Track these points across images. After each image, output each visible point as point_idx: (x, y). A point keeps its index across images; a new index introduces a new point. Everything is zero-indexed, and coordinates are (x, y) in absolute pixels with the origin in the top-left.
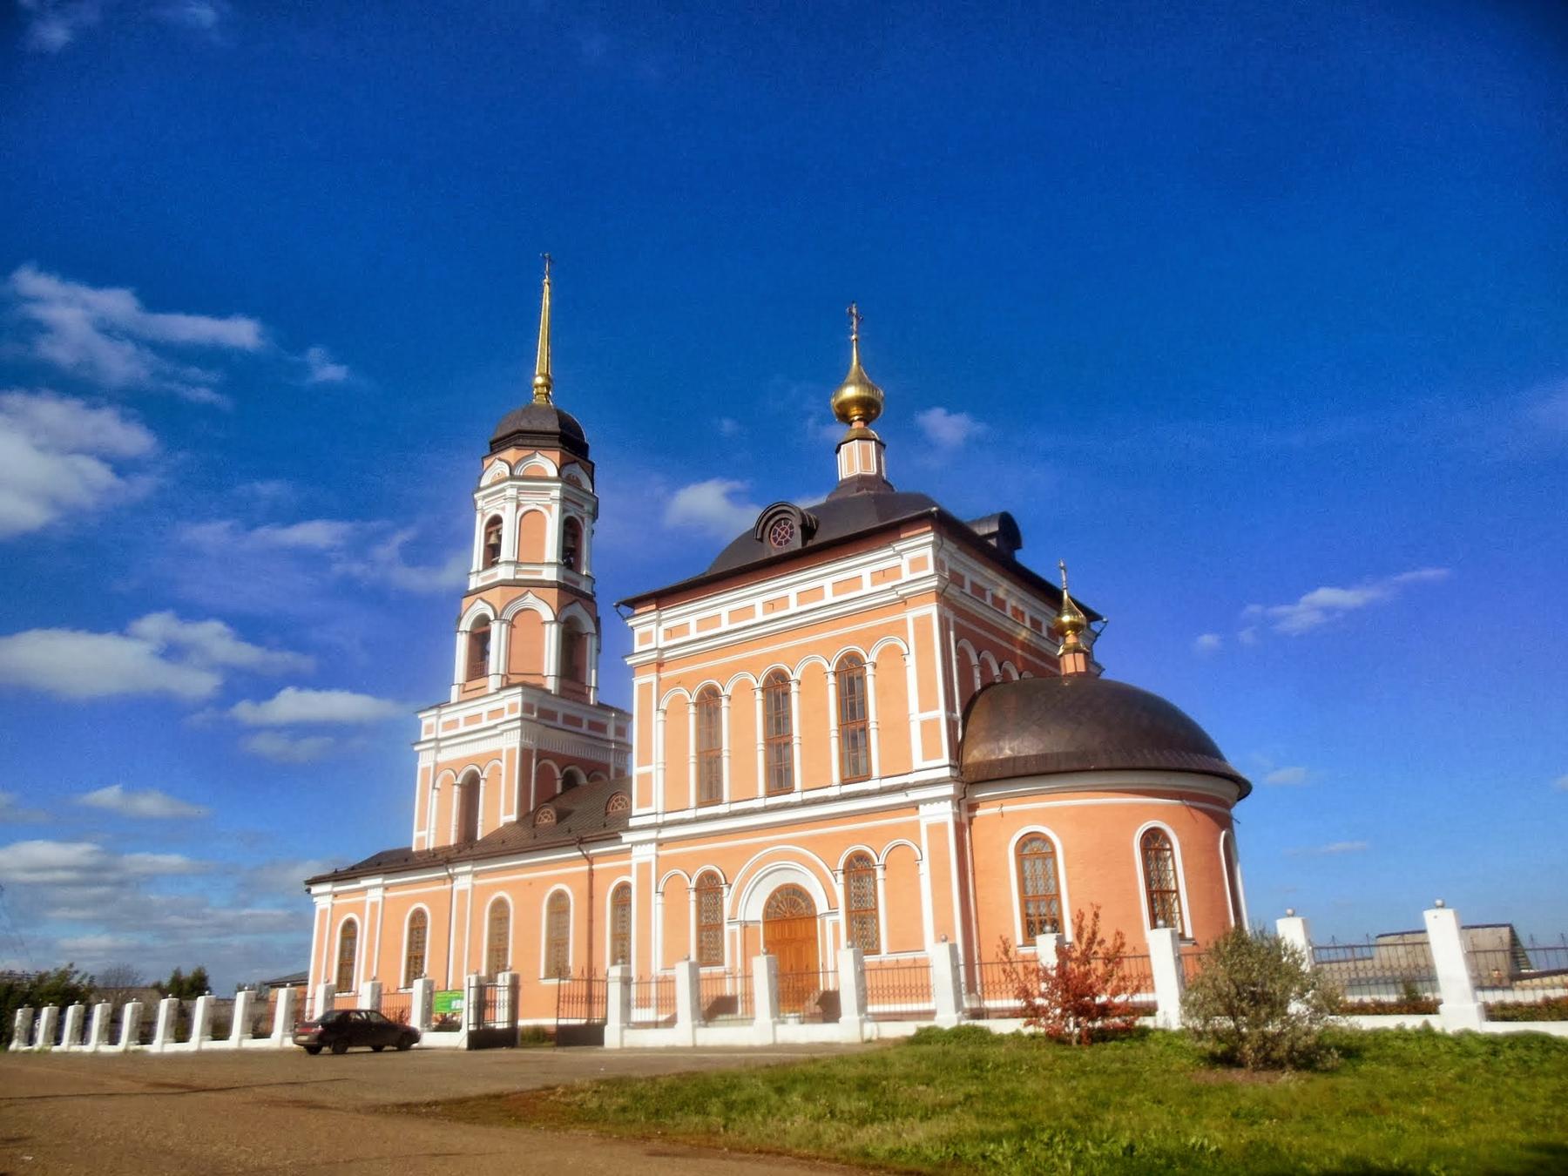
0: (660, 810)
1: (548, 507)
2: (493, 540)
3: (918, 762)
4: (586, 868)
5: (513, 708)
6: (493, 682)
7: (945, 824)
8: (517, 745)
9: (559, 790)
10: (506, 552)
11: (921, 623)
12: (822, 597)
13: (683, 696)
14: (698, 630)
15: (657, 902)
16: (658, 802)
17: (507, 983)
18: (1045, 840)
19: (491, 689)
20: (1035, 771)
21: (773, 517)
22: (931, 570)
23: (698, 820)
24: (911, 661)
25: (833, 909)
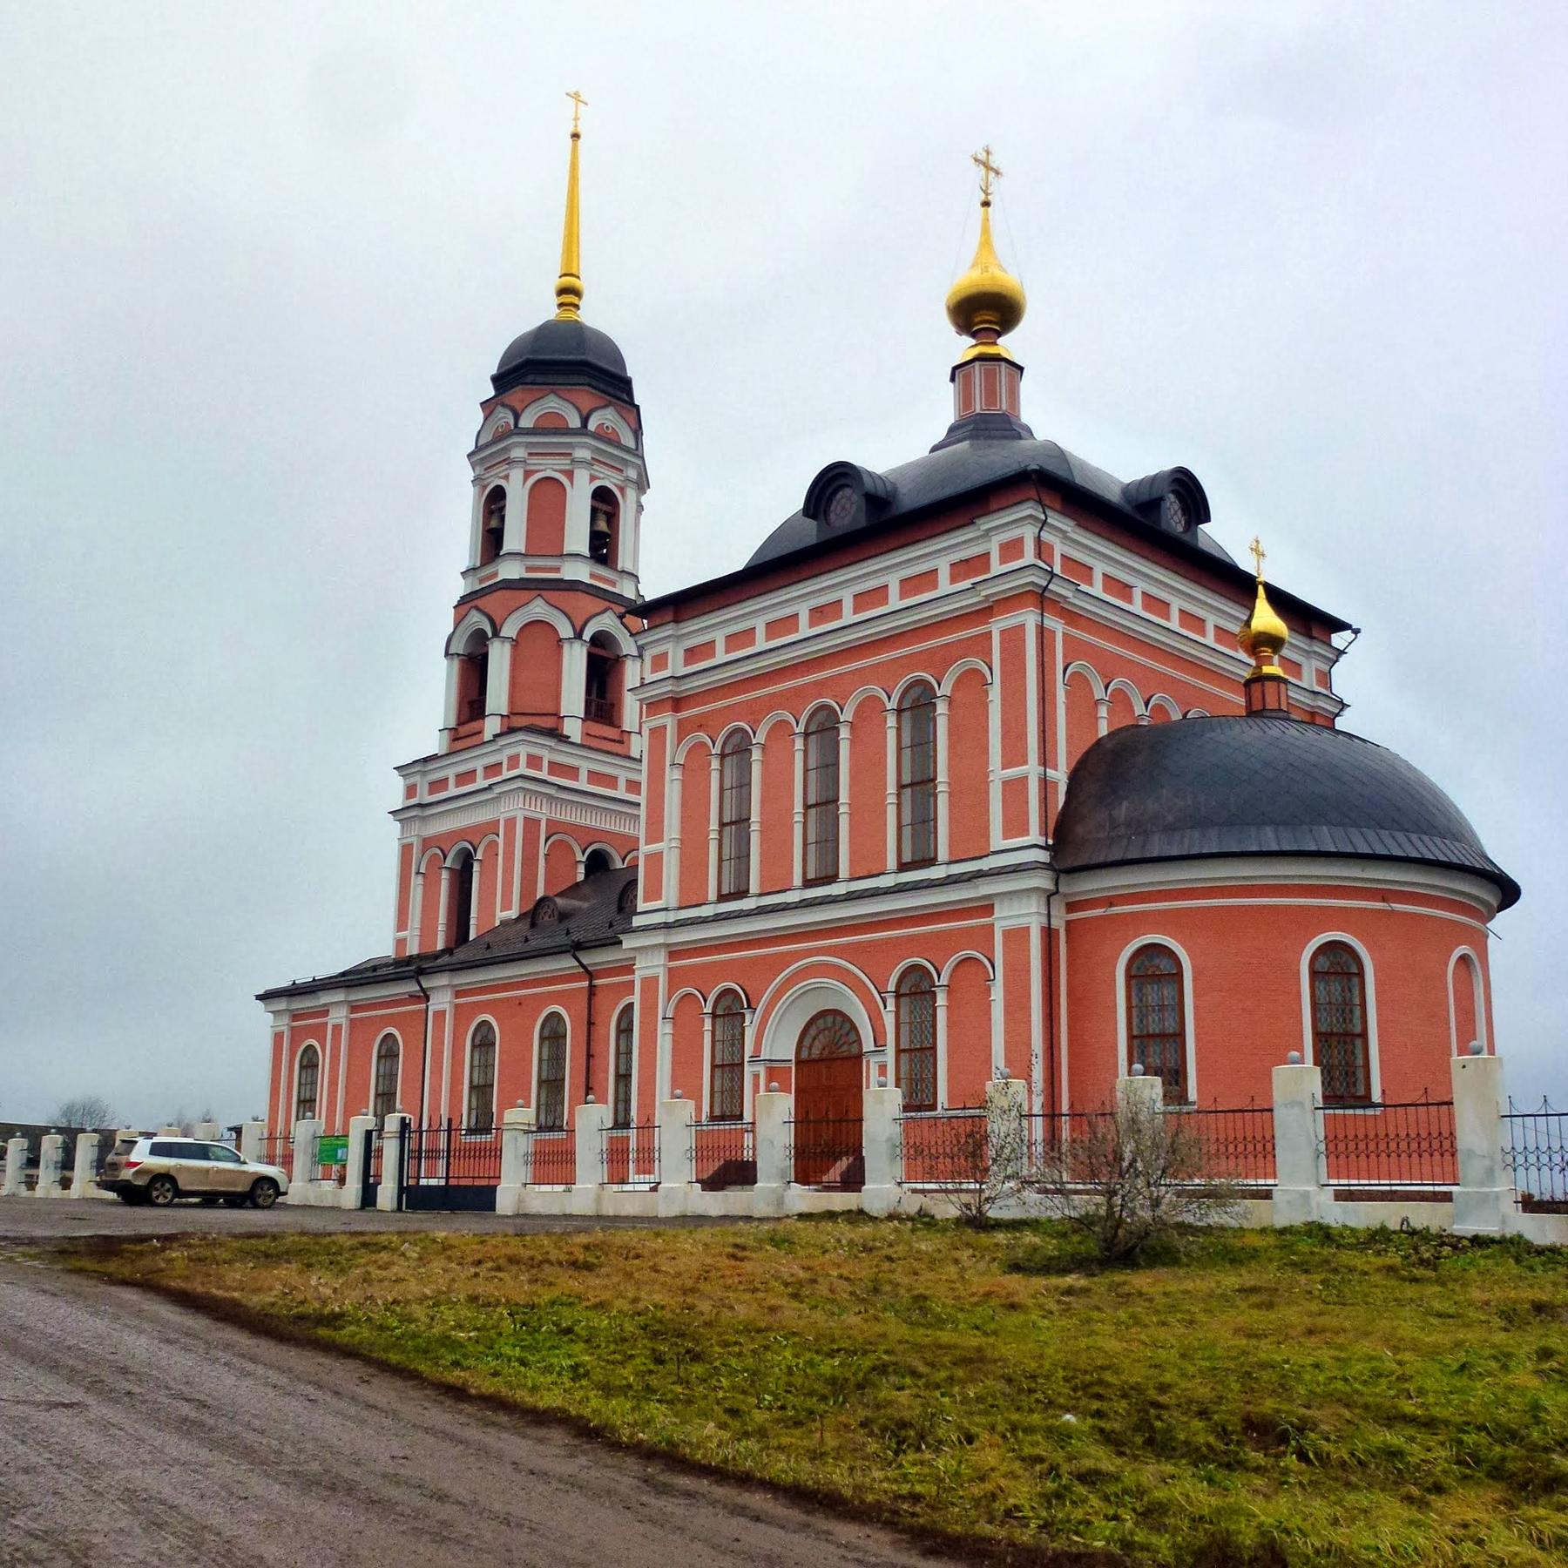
0: (673, 903)
2: (494, 523)
3: (997, 841)
4: (586, 984)
6: (491, 726)
9: (581, 877)
10: (514, 539)
12: (885, 601)
13: (703, 744)
14: (856, 611)
15: (664, 1031)
16: (670, 892)
19: (487, 736)
23: (718, 918)
25: (879, 1040)
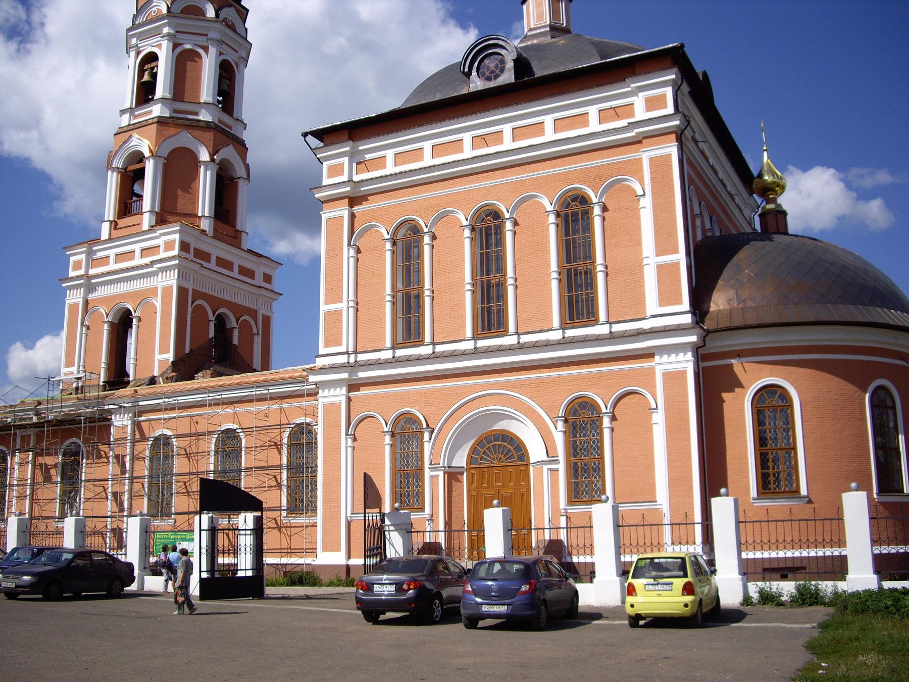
1: (206, 49)
2: (146, 77)
3: (652, 305)
5: (169, 246)
7: (684, 373)
8: (174, 283)
10: (161, 90)
11: (660, 165)
16: (347, 343)
17: (250, 525)
18: (594, 406)
20: (754, 322)
21: (480, 54)
22: (670, 109)
24: (646, 203)
